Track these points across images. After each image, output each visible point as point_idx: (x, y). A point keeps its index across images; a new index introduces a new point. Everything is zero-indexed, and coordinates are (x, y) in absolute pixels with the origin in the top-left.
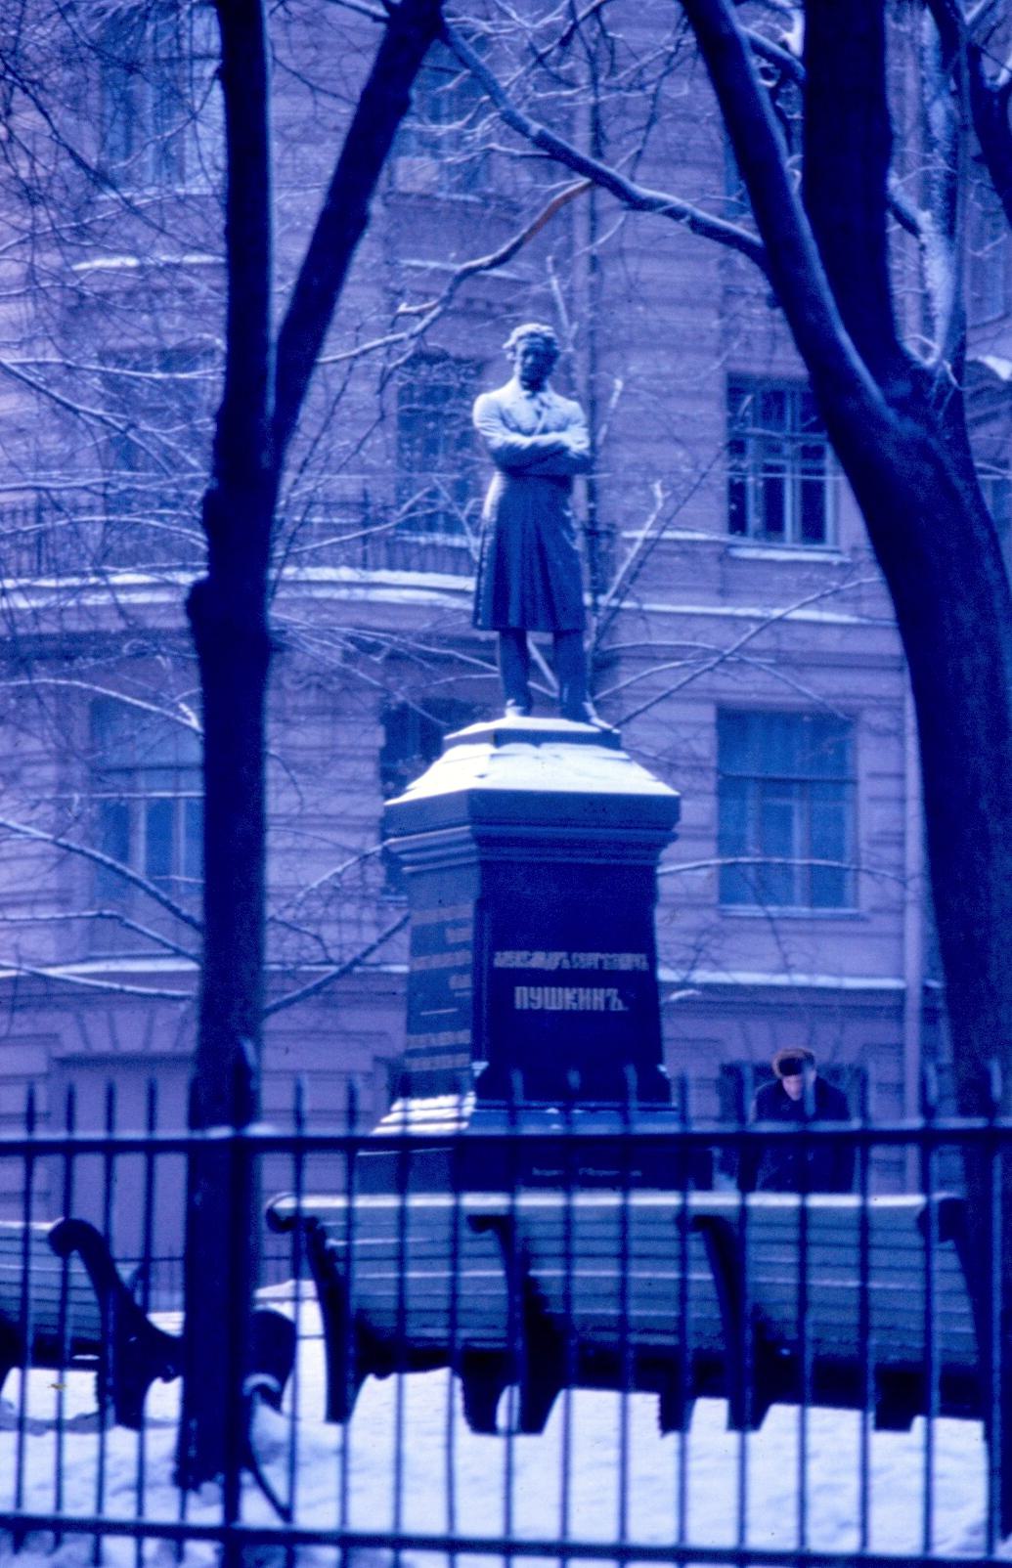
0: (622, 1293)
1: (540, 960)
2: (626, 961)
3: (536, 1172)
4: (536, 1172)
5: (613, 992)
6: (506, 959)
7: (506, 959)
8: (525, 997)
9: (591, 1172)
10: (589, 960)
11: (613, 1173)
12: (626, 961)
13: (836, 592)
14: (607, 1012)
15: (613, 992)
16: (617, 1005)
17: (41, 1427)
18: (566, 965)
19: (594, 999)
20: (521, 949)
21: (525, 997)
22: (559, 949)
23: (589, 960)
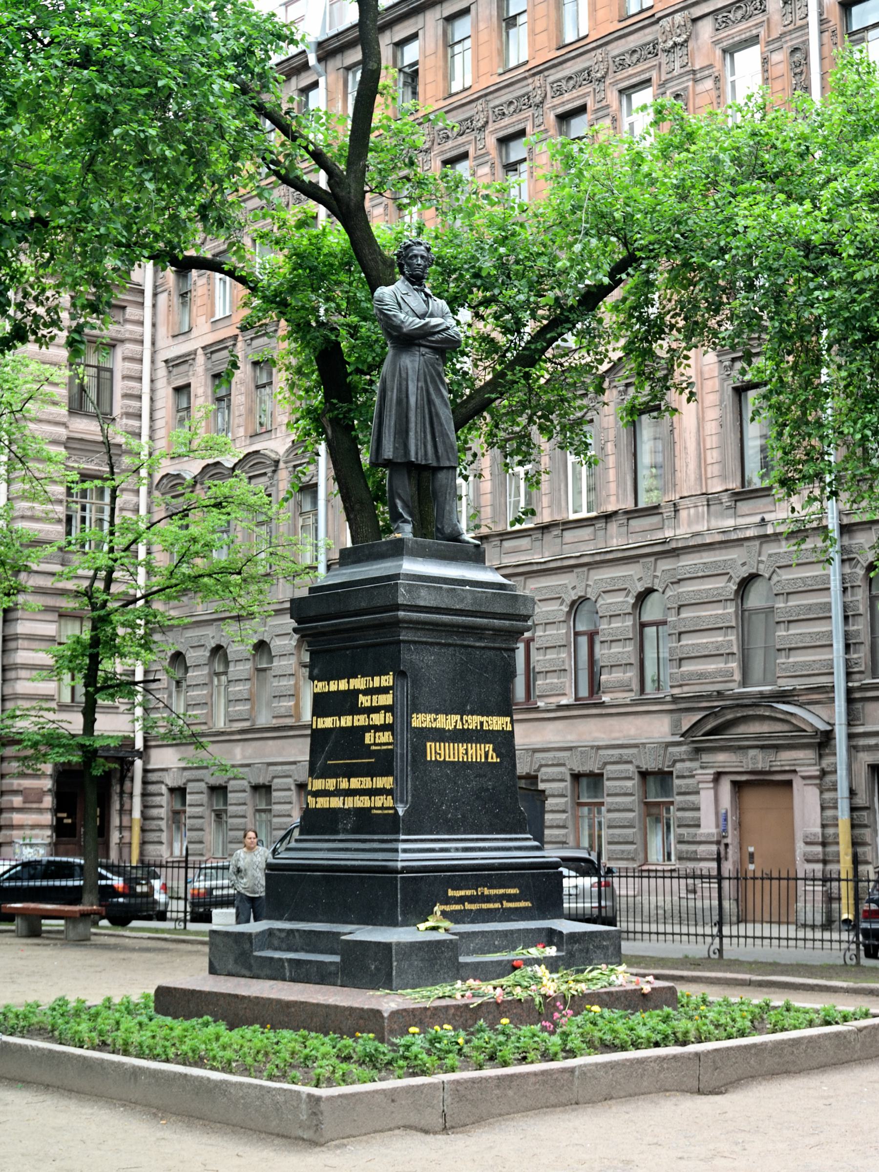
0: (847, 880)
1: (448, 722)
2: (497, 723)
3: (451, 893)
4: (451, 893)
5: (490, 747)
6: (419, 721)
7: (419, 721)
8: (435, 751)
9: (487, 892)
10: (473, 721)
11: (343, 937)
12: (497, 723)
13: (365, 319)
14: (486, 763)
15: (490, 747)
16: (493, 758)
17: (792, 923)
18: (459, 726)
19: (477, 752)
20: (430, 713)
21: (435, 751)
22: (456, 714)
23: (473, 721)
